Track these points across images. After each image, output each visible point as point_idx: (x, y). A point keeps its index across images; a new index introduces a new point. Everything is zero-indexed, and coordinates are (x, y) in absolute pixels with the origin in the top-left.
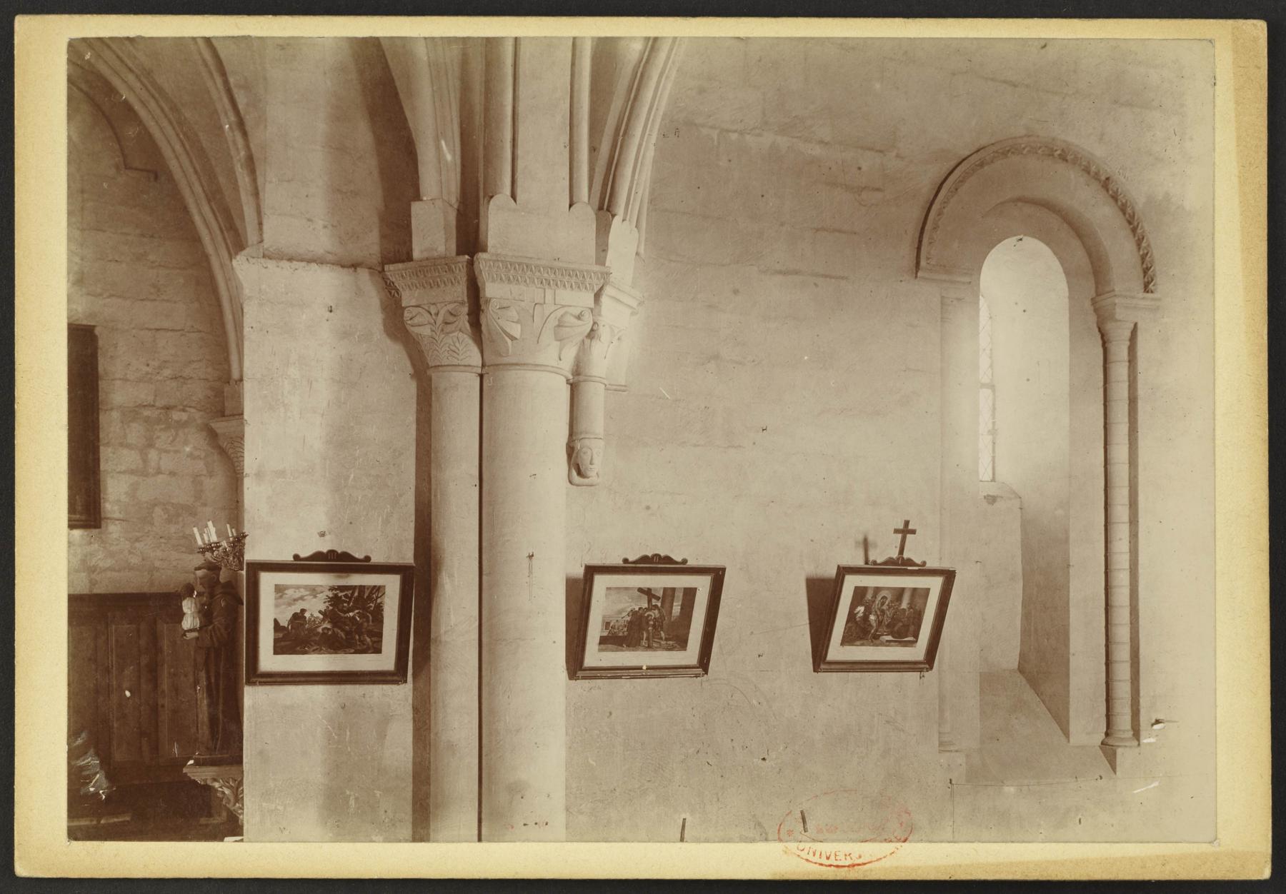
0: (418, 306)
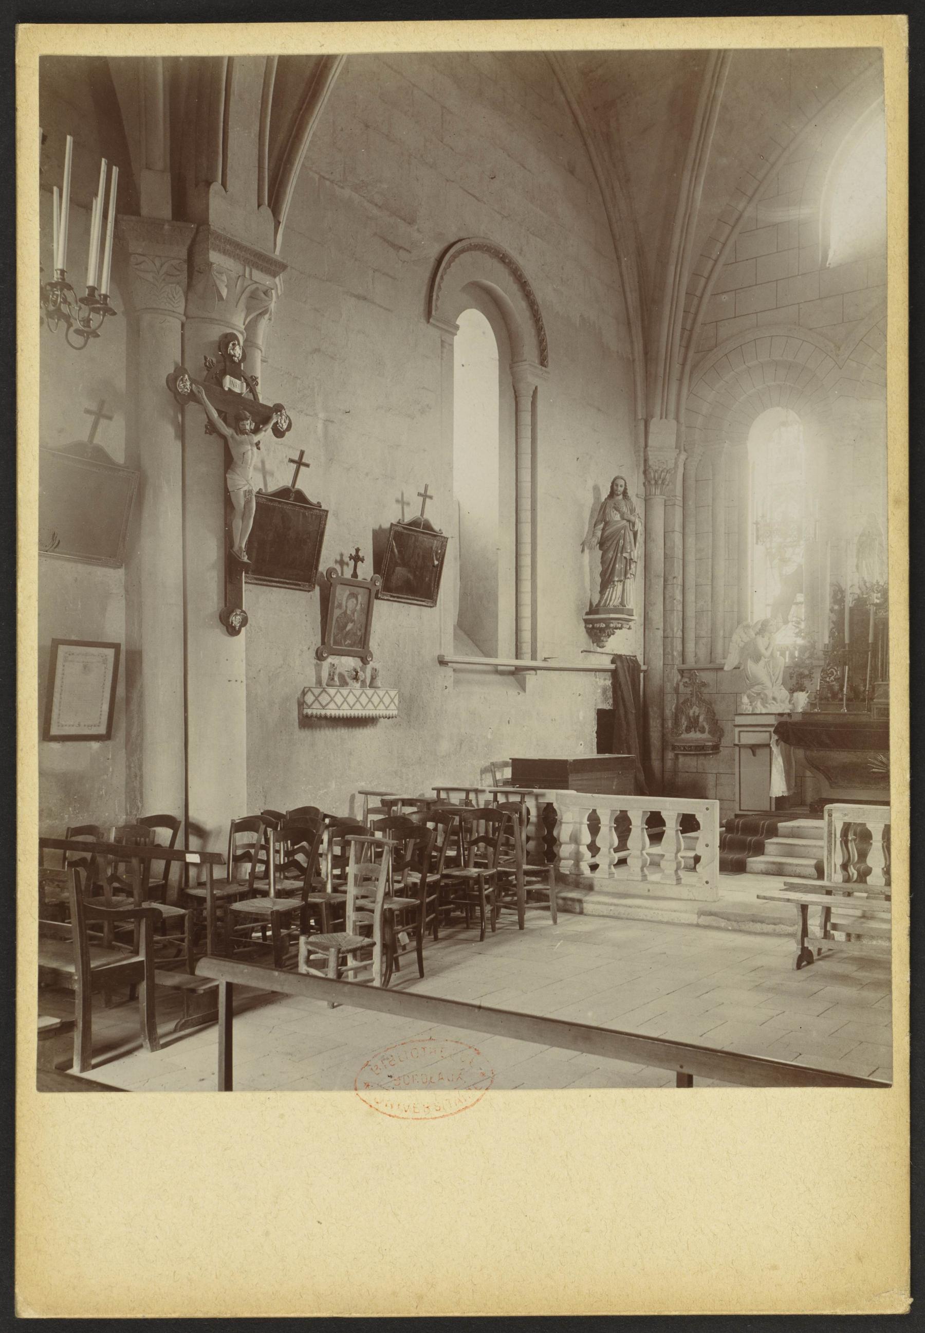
0: (143, 255)
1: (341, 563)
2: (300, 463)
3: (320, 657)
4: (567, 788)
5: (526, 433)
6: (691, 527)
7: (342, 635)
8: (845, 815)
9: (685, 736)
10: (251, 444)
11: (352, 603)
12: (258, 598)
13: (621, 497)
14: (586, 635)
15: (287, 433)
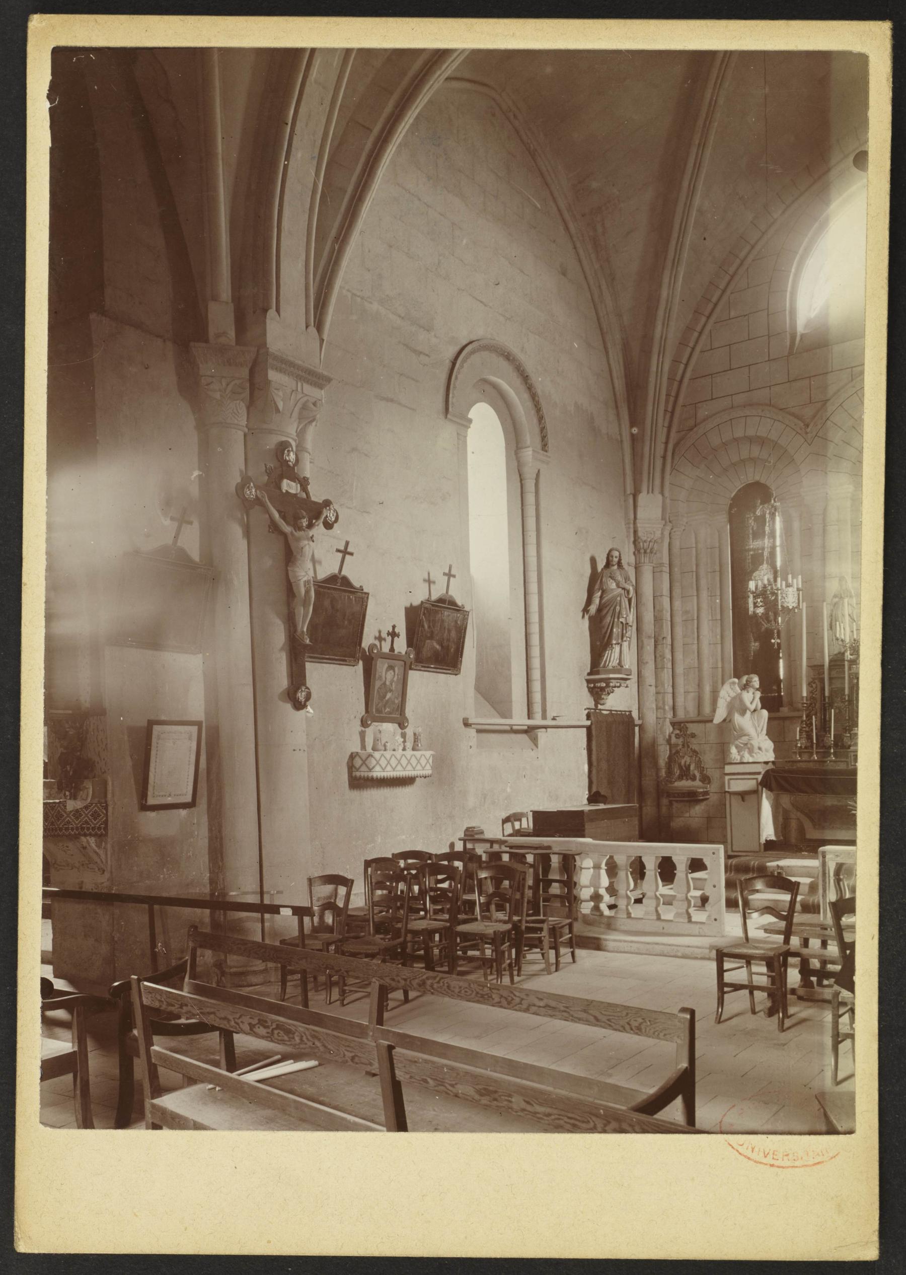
1: (380, 638)
2: (345, 552)
3: (364, 723)
4: (583, 836)
5: (531, 511)
6: (677, 591)
7: (383, 706)
8: (837, 856)
9: (677, 784)
10: (308, 539)
11: (390, 675)
12: (319, 674)
13: (616, 567)
14: (589, 694)
15: (335, 525)
